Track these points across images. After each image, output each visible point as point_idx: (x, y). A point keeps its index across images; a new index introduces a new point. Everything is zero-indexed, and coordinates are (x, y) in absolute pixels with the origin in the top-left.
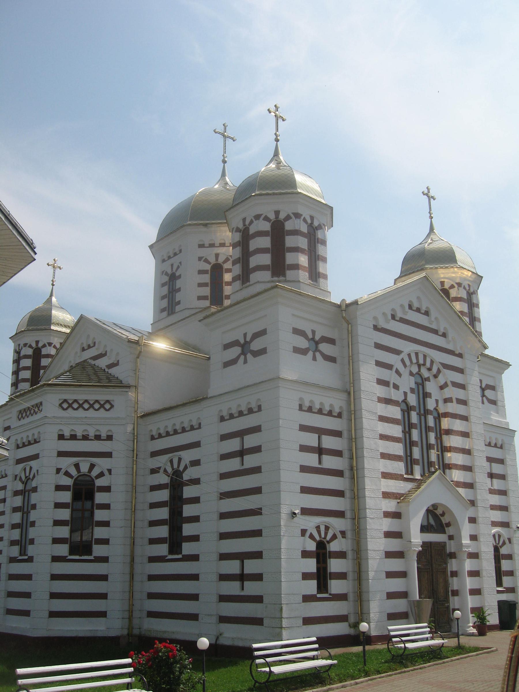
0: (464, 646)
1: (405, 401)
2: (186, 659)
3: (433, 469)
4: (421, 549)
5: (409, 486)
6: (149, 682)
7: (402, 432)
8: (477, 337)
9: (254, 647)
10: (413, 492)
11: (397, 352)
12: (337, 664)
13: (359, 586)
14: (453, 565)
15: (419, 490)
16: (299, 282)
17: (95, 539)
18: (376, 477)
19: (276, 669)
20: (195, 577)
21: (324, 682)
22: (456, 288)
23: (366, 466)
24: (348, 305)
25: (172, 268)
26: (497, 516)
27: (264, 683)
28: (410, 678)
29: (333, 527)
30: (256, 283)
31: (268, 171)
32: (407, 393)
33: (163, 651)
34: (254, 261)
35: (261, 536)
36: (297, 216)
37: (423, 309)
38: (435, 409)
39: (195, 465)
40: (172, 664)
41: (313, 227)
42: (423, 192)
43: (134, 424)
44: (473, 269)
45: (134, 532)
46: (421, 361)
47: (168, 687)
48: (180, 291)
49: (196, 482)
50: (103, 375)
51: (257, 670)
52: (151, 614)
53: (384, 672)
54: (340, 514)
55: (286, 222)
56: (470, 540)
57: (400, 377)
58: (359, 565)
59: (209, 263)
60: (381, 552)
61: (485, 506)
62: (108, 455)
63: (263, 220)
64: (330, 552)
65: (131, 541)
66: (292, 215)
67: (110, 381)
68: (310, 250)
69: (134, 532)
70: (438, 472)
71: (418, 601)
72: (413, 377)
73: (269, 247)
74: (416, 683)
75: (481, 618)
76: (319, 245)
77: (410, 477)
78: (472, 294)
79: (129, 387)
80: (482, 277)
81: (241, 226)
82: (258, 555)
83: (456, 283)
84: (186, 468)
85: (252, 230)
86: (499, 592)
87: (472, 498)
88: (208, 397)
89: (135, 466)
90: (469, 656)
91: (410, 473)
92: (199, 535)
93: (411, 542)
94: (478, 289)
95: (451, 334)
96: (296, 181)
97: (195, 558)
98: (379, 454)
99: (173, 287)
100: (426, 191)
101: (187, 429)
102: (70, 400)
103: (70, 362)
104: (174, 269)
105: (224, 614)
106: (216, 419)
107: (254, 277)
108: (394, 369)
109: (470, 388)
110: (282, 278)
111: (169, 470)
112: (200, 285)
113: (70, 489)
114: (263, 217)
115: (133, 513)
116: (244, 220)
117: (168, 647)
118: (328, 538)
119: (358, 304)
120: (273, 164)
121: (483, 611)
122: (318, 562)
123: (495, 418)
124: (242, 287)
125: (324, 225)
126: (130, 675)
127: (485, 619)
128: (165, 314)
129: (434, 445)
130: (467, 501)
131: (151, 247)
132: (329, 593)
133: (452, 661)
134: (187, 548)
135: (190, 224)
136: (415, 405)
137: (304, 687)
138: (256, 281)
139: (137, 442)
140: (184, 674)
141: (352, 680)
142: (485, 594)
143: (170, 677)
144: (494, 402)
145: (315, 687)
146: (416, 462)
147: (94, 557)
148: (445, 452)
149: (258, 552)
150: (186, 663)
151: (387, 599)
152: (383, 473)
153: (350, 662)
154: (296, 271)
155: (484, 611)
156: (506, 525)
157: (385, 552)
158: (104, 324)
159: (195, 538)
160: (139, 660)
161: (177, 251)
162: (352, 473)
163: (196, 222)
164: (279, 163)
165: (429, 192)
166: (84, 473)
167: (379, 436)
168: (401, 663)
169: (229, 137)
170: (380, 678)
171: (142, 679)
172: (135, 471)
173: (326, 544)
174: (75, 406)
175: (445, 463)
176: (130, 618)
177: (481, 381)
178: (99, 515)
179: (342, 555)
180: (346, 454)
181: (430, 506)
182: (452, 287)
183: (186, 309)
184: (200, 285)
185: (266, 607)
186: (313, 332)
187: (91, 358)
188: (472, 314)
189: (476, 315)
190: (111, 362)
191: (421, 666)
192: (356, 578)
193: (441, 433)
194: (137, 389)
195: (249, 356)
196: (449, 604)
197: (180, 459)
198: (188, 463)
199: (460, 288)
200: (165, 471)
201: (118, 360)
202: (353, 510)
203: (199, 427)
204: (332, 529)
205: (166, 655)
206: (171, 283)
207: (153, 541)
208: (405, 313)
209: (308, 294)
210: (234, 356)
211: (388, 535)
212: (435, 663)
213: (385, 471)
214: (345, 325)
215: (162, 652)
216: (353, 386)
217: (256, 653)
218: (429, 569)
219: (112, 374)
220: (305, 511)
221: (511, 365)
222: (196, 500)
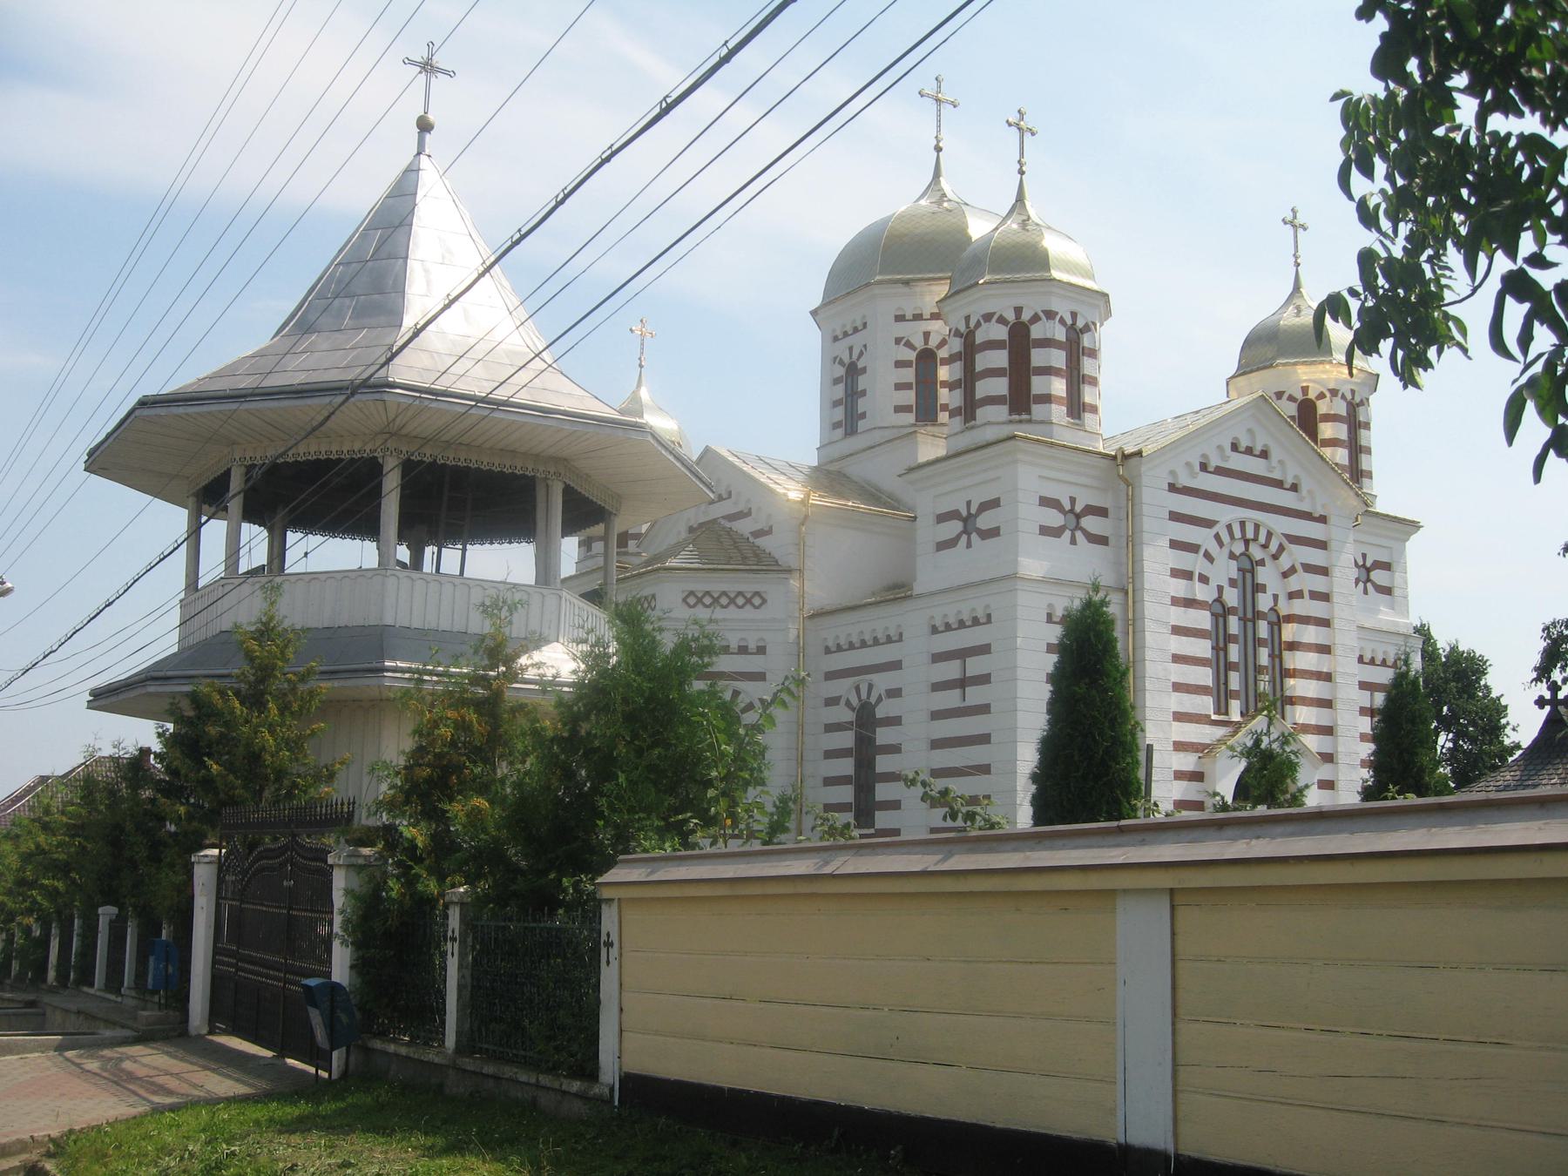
1: (1219, 600)
5: (1220, 732)
11: (1208, 523)
30: (985, 424)
34: (984, 388)
36: (1050, 315)
37: (1258, 449)
39: (894, 697)
42: (1283, 220)
46: (1250, 535)
48: (865, 372)
49: (895, 721)
63: (997, 322)
66: (1041, 315)
76: (1085, 358)
78: (1358, 405)
79: (789, 571)
83: (1329, 390)
84: (880, 699)
85: (980, 338)
91: (1223, 710)
98: (1171, 684)
100: (1289, 217)
101: (881, 641)
104: (855, 357)
107: (984, 413)
109: (1336, 573)
110: (1024, 417)
112: (899, 387)
114: (996, 317)
119: (1142, 456)
123: (1386, 617)
128: (840, 432)
131: (814, 313)
136: (1236, 605)
144: (1387, 591)
146: (1235, 695)
154: (1047, 405)
161: (859, 324)
164: (1024, 224)
165: (1295, 217)
169: (946, 101)
177: (1364, 556)
182: (1321, 396)
183: (875, 428)
184: (899, 387)
186: (1073, 500)
190: (758, 527)
197: (870, 687)
198: (883, 693)
200: (848, 704)
201: (770, 524)
214: (1123, 486)
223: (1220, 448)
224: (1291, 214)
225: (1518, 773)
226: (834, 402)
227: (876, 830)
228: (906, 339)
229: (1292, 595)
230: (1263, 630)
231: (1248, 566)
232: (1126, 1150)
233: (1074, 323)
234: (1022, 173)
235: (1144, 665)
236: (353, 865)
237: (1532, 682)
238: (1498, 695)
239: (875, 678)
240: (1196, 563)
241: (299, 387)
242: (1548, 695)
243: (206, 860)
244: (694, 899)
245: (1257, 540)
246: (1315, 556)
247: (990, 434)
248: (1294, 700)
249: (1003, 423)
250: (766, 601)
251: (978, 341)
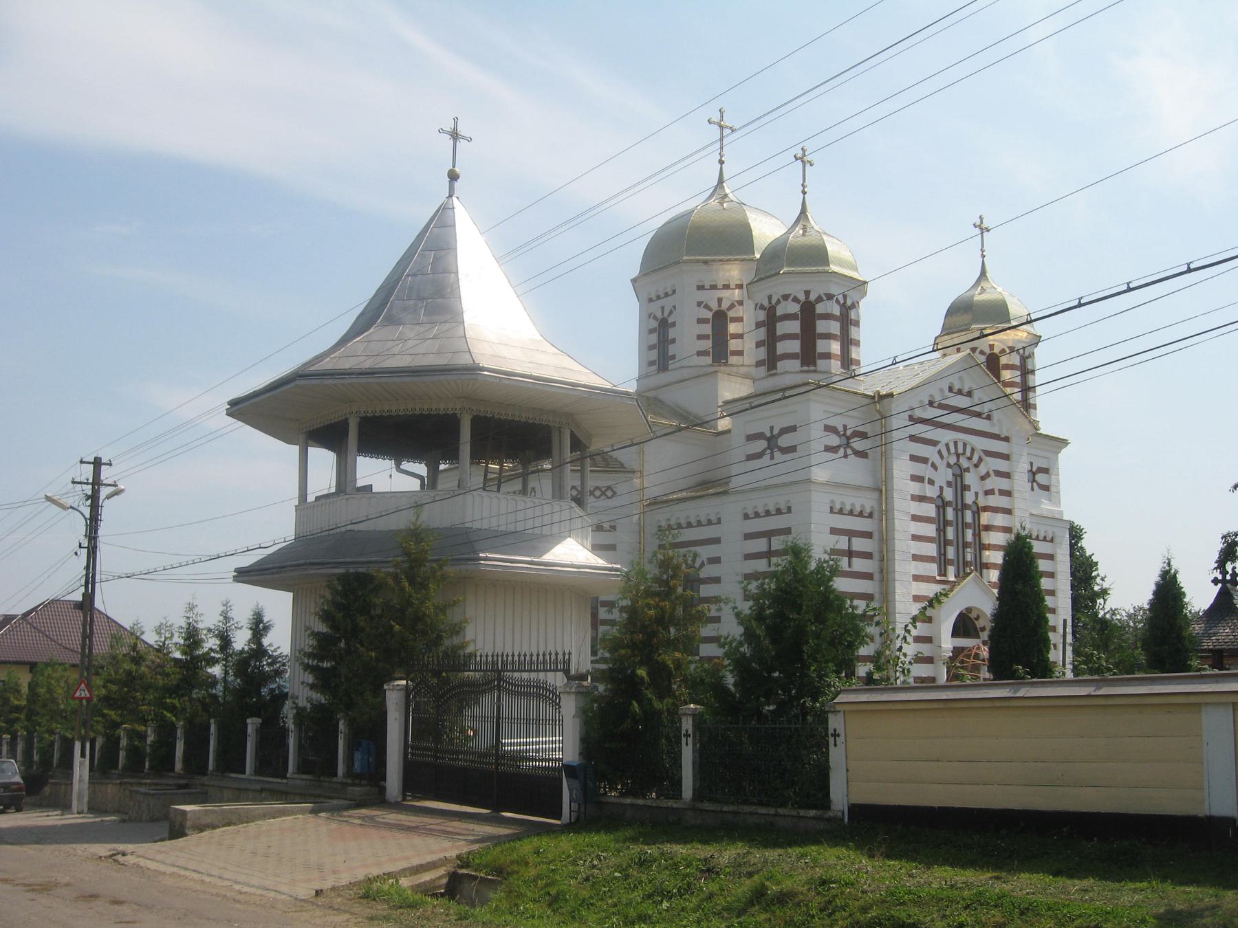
1: (940, 496)
3: (968, 570)
11: (934, 443)
23: (897, 569)
25: (663, 312)
34: (783, 347)
36: (830, 297)
42: (974, 224)
46: (960, 450)
57: (936, 470)
59: (711, 310)
76: (852, 327)
78: (1027, 358)
79: (633, 472)
84: (702, 565)
91: (943, 573)
99: (664, 336)
108: (930, 462)
109: (1016, 476)
110: (812, 368)
112: (700, 337)
123: (1046, 507)
128: (655, 368)
144: (1046, 488)
146: (951, 562)
152: (915, 597)
154: (828, 360)
165: (982, 223)
177: (1031, 464)
180: (876, 556)
182: (1003, 351)
184: (700, 337)
193: (980, 529)
223: (941, 390)
224: (979, 220)
225: (1203, 625)
228: (704, 303)
229: (987, 493)
230: (969, 516)
231: (958, 472)
232: (1210, 819)
233: (845, 302)
234: (804, 193)
235: (894, 542)
236: (580, 693)
237: (1214, 569)
238: (1090, 554)
240: (924, 470)
241: (416, 368)
242: (1220, 577)
243: (399, 688)
244: (973, 708)
245: (971, 459)
246: (1002, 465)
247: (788, 380)
248: (988, 565)
249: (797, 372)
250: (597, 487)
251: (778, 313)
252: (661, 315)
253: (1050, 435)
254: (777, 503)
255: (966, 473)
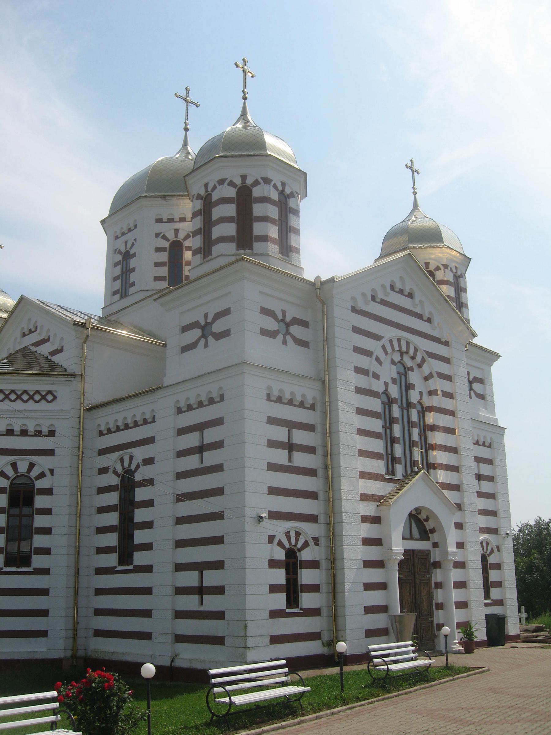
0: (453, 666)
1: (386, 392)
2: (126, 690)
4: (402, 557)
6: (79, 720)
7: (383, 427)
8: (465, 324)
9: (211, 673)
10: (394, 494)
11: (378, 338)
12: (310, 691)
13: (334, 599)
14: (437, 575)
15: (401, 492)
16: (268, 255)
17: (35, 548)
18: (354, 476)
19: (238, 700)
20: (148, 591)
21: (295, 713)
22: (442, 270)
24: (323, 283)
26: (484, 521)
27: (224, 716)
28: (395, 706)
29: (304, 533)
30: (219, 256)
31: (233, 131)
32: (388, 383)
33: (97, 681)
34: (217, 232)
35: (223, 543)
36: (267, 181)
38: (420, 402)
40: (108, 697)
41: (284, 195)
43: (80, 418)
44: (460, 250)
45: (79, 540)
46: (404, 349)
47: (104, 725)
50: (46, 362)
51: (215, 701)
52: (99, 633)
53: (365, 699)
54: (312, 519)
55: (254, 188)
56: (457, 548)
58: (334, 576)
60: (358, 561)
61: (473, 511)
62: (50, 453)
64: (301, 561)
65: (76, 551)
66: (261, 181)
67: (53, 369)
68: (281, 220)
69: (79, 540)
70: (422, 471)
71: (399, 615)
72: (395, 366)
73: (234, 216)
74: (403, 712)
75: (469, 633)
76: (291, 215)
77: (391, 477)
78: (459, 277)
80: (470, 259)
81: (202, 192)
82: (219, 565)
83: (442, 265)
84: (138, 467)
85: (215, 196)
86: (486, 605)
87: (458, 502)
88: (164, 387)
89: (80, 465)
90: (459, 678)
91: (390, 473)
92: (153, 543)
93: (392, 549)
94: (466, 272)
95: (436, 320)
96: (266, 142)
97: (148, 569)
98: (357, 450)
101: (139, 423)
102: (7, 390)
103: (9, 349)
104: (128, 247)
105: (180, 633)
106: (173, 410)
107: (217, 249)
109: (457, 379)
110: (248, 251)
111: (120, 470)
112: (157, 264)
113: (7, 492)
114: (227, 182)
115: (78, 519)
116: (206, 185)
117: (105, 676)
118: (299, 545)
119: (334, 282)
120: (240, 124)
121: (471, 626)
122: (287, 573)
123: (483, 414)
124: (203, 261)
125: (297, 193)
126: (54, 712)
127: (473, 635)
129: (417, 442)
130: (453, 505)
131: (103, 222)
132: (300, 607)
133: (441, 683)
134: (139, 558)
135: (146, 196)
137: (271, 720)
138: (219, 254)
139: (83, 438)
140: (123, 709)
141: (328, 709)
142: (472, 607)
143: (106, 714)
144: (482, 397)
145: (285, 719)
147: (34, 569)
148: (429, 450)
149: (219, 561)
150: (126, 695)
151: (365, 614)
152: (361, 473)
153: (325, 686)
154: (265, 243)
155: (472, 626)
156: (494, 531)
157: (364, 561)
158: (47, 306)
159: (148, 547)
160: (67, 692)
161: (132, 226)
162: (327, 472)
163: (153, 194)
164: (247, 122)
165: (412, 165)
166: (22, 474)
167: (357, 431)
168: (383, 687)
170: (360, 706)
171: (69, 717)
172: (80, 471)
173: (296, 552)
174: (13, 397)
175: (429, 462)
176: (75, 638)
177: (468, 373)
178: (40, 521)
179: (314, 564)
180: (320, 451)
181: (413, 509)
182: (438, 268)
184: (157, 264)
185: (228, 624)
186: (284, 313)
187: (32, 345)
188: (459, 298)
189: (464, 301)
191: (406, 690)
192: (331, 591)
194: (83, 379)
195: (211, 339)
196: (432, 619)
197: (131, 458)
199: (446, 270)
202: (327, 514)
203: (154, 421)
204: (303, 535)
205: (101, 686)
206: (125, 262)
207: (101, 551)
208: (387, 294)
209: (279, 270)
210: (219, 322)
211: (367, 542)
212: (422, 686)
213: (363, 471)
214: (319, 305)
215: (96, 683)
216: (328, 374)
217: (214, 681)
218: (412, 580)
219: (55, 362)
220: (274, 515)
221: (501, 356)
222: (149, 503)
226: (114, 278)
227: (134, 566)
234: (245, 98)
239: (135, 451)
246: (443, 368)
252: (124, 248)
253: (484, 346)
254: (210, 392)
255: (410, 372)
